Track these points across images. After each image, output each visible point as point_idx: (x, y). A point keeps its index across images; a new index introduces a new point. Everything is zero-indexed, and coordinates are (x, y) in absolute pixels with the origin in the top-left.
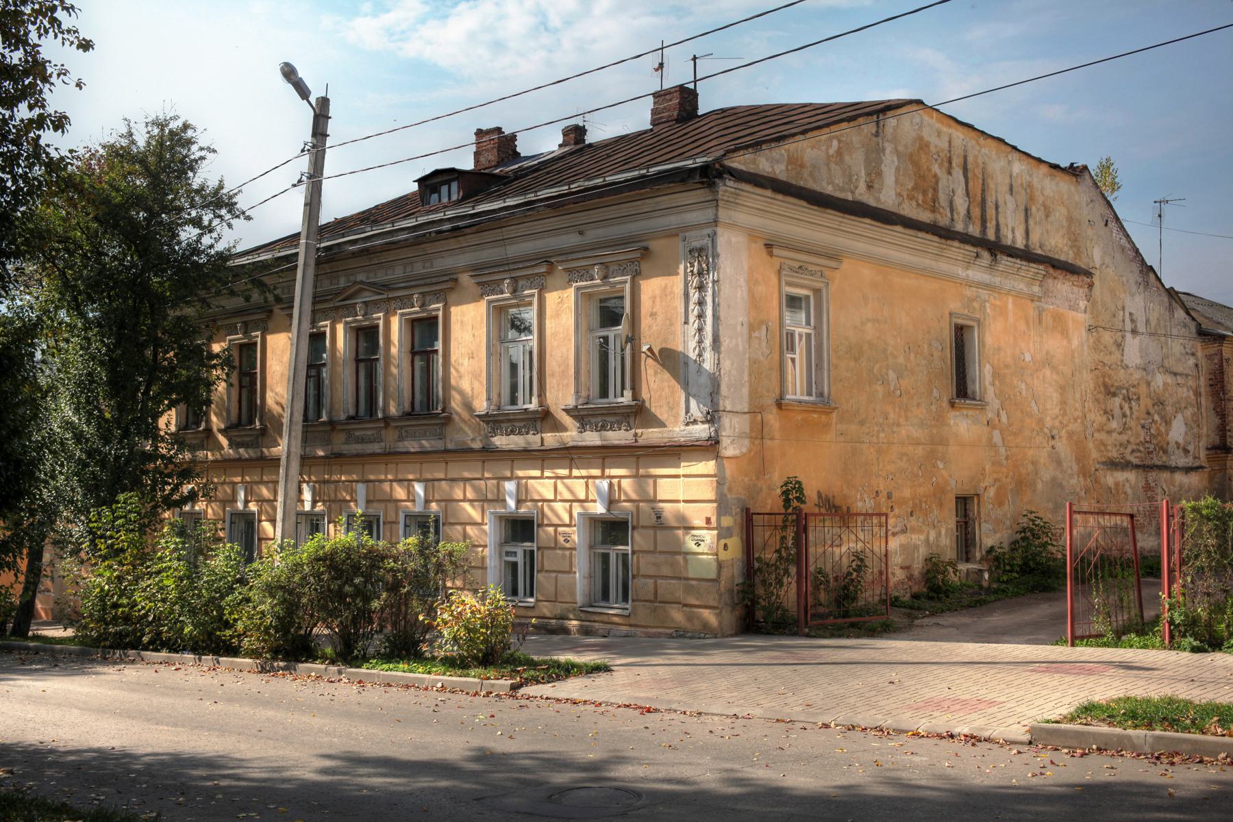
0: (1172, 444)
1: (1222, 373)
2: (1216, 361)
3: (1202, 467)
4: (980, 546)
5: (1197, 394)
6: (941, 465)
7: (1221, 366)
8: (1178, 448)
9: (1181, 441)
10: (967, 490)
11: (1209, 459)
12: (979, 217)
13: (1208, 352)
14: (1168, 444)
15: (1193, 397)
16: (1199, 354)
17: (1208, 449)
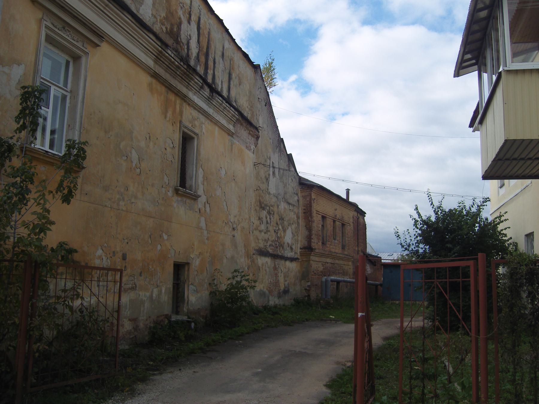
0: (286, 244)
1: (311, 206)
2: (308, 199)
3: (297, 259)
4: (188, 303)
5: (298, 217)
6: (165, 237)
7: (310, 202)
8: (288, 246)
9: (290, 243)
10: (181, 259)
11: (301, 254)
12: (204, 63)
13: (303, 194)
14: (284, 243)
15: (296, 219)
16: (299, 194)
17: (301, 248)
